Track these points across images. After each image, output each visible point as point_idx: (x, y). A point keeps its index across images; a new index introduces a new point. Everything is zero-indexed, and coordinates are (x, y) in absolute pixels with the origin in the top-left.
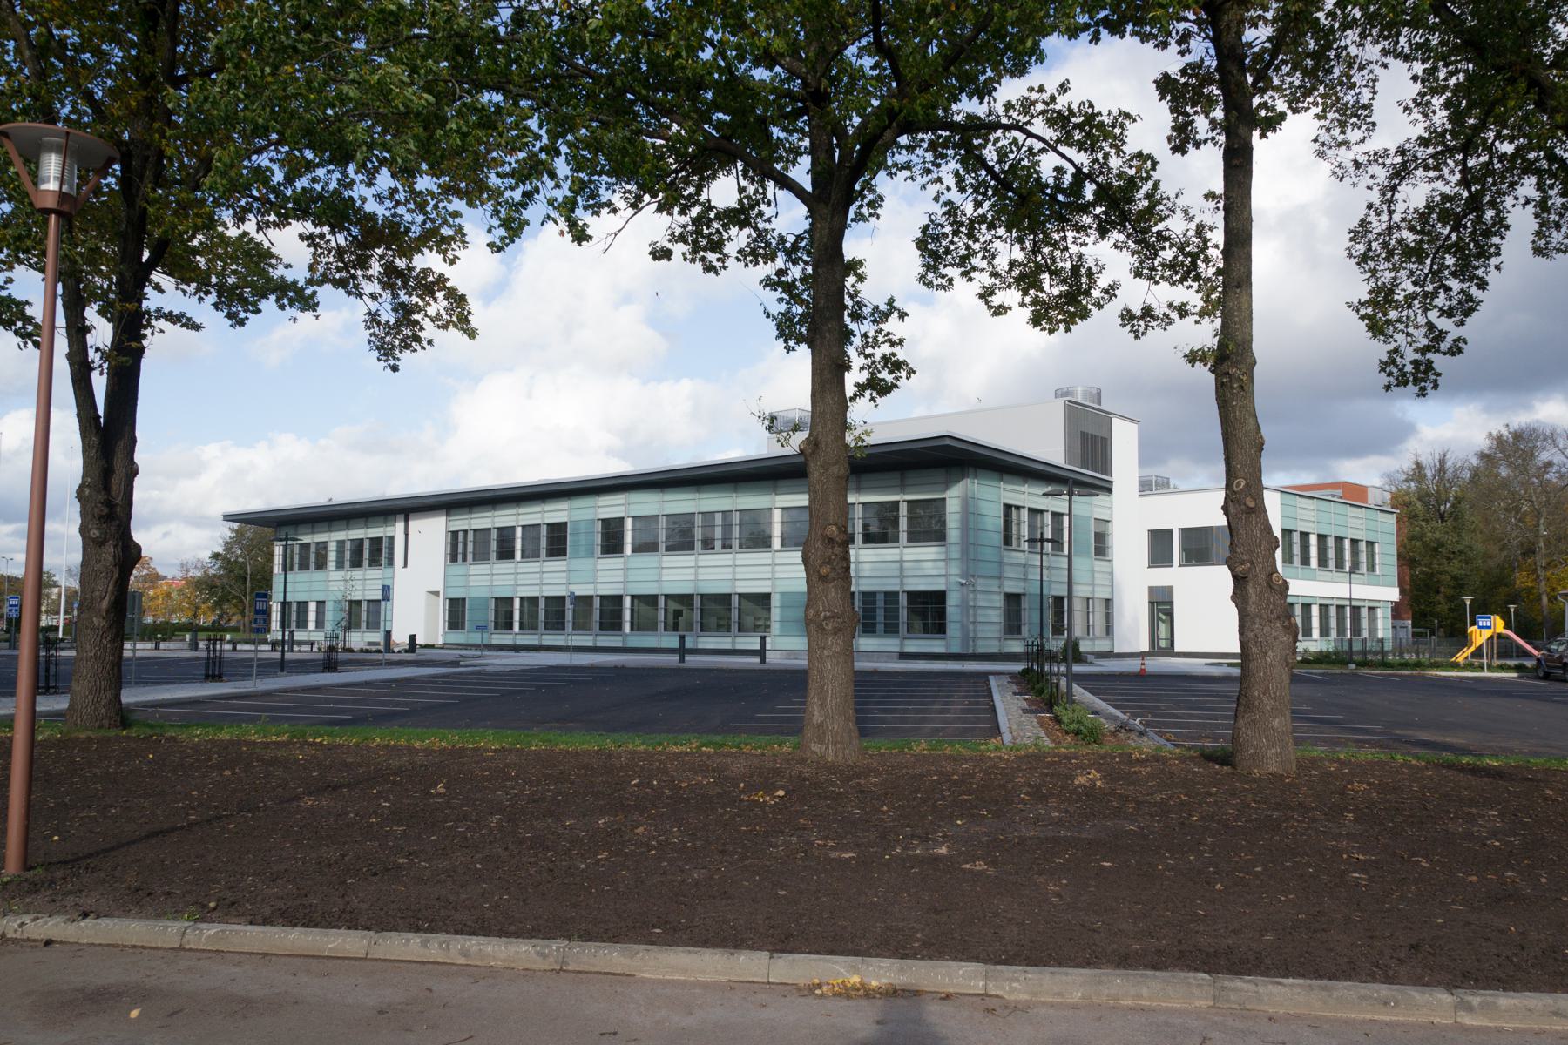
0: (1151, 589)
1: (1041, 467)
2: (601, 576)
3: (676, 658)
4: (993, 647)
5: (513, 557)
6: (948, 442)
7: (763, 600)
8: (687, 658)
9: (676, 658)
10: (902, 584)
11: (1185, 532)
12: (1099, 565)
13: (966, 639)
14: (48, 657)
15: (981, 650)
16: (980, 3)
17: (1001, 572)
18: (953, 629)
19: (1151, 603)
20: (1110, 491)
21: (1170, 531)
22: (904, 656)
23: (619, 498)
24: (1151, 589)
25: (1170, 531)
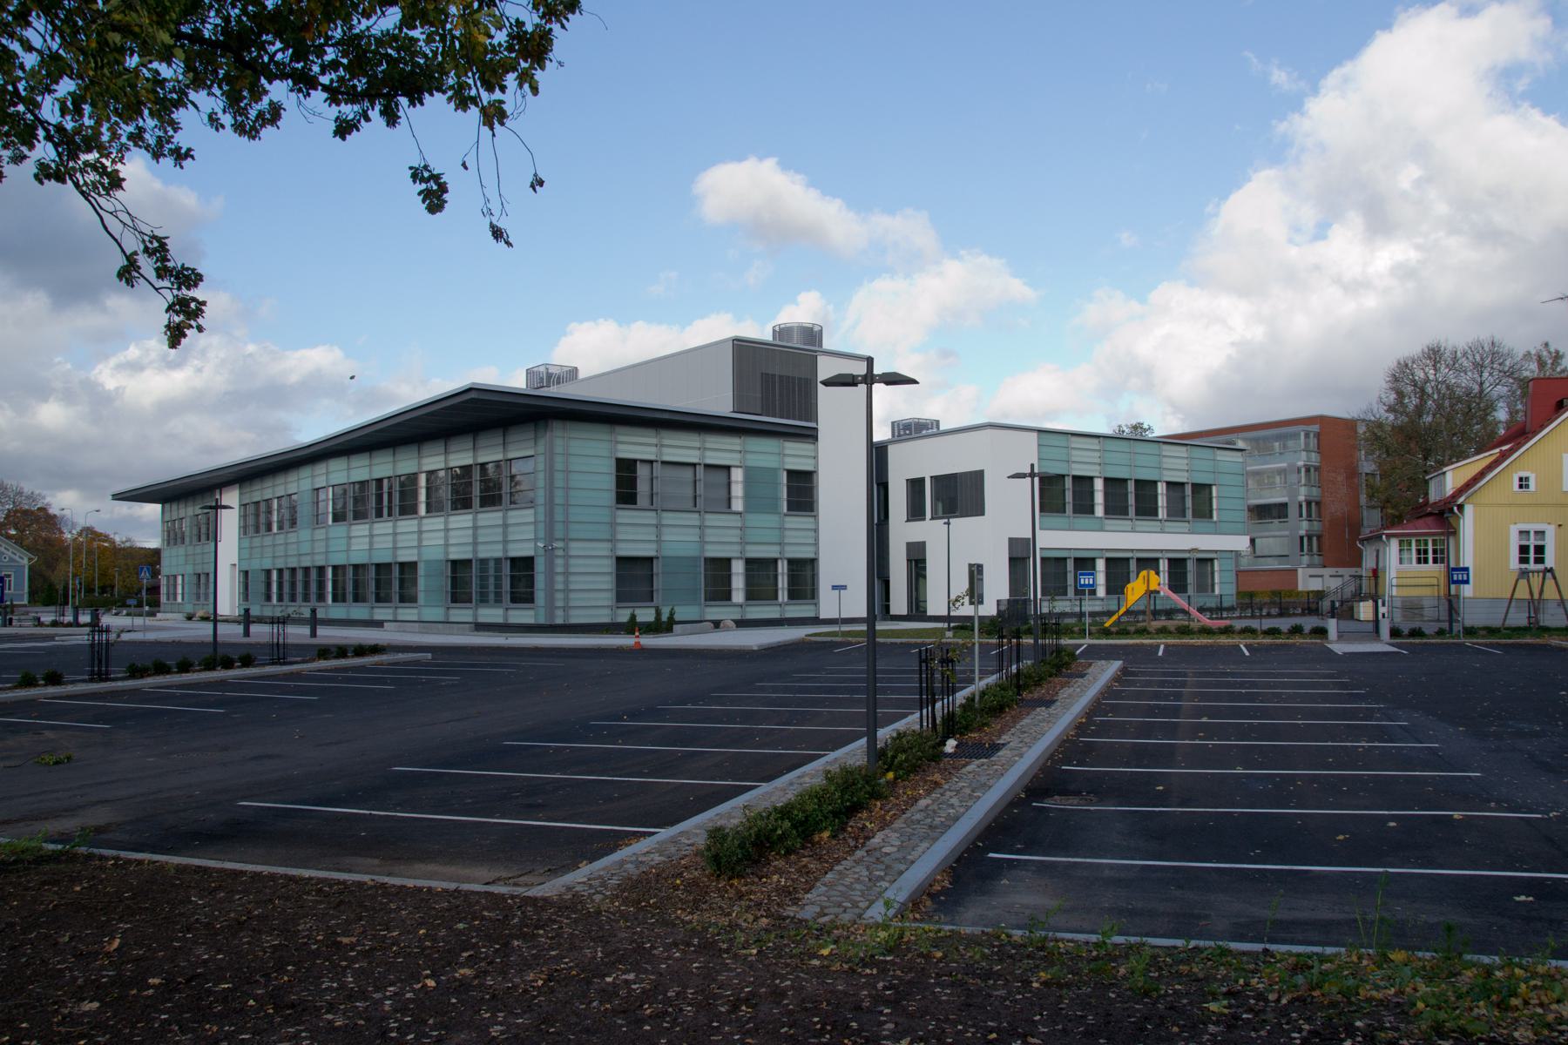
0: (1011, 540)
1: (666, 416)
2: (790, 537)
3: (306, 630)
4: (603, 617)
5: (1092, 511)
6: (473, 395)
7: (409, 568)
8: (321, 631)
9: (306, 630)
10: (505, 550)
11: (936, 480)
12: (798, 522)
13: (551, 607)
14: (1018, 645)
15: (573, 621)
16: (127, 5)
17: (614, 533)
18: (540, 596)
19: (1011, 559)
20: (815, 438)
21: (923, 480)
22: (480, 627)
23: (733, 443)
24: (1011, 540)
25: (923, 480)
